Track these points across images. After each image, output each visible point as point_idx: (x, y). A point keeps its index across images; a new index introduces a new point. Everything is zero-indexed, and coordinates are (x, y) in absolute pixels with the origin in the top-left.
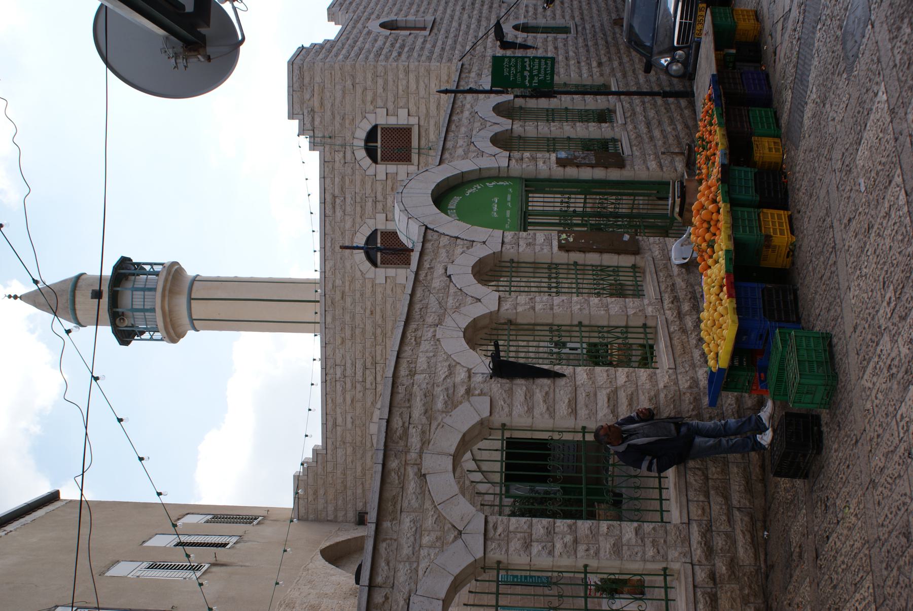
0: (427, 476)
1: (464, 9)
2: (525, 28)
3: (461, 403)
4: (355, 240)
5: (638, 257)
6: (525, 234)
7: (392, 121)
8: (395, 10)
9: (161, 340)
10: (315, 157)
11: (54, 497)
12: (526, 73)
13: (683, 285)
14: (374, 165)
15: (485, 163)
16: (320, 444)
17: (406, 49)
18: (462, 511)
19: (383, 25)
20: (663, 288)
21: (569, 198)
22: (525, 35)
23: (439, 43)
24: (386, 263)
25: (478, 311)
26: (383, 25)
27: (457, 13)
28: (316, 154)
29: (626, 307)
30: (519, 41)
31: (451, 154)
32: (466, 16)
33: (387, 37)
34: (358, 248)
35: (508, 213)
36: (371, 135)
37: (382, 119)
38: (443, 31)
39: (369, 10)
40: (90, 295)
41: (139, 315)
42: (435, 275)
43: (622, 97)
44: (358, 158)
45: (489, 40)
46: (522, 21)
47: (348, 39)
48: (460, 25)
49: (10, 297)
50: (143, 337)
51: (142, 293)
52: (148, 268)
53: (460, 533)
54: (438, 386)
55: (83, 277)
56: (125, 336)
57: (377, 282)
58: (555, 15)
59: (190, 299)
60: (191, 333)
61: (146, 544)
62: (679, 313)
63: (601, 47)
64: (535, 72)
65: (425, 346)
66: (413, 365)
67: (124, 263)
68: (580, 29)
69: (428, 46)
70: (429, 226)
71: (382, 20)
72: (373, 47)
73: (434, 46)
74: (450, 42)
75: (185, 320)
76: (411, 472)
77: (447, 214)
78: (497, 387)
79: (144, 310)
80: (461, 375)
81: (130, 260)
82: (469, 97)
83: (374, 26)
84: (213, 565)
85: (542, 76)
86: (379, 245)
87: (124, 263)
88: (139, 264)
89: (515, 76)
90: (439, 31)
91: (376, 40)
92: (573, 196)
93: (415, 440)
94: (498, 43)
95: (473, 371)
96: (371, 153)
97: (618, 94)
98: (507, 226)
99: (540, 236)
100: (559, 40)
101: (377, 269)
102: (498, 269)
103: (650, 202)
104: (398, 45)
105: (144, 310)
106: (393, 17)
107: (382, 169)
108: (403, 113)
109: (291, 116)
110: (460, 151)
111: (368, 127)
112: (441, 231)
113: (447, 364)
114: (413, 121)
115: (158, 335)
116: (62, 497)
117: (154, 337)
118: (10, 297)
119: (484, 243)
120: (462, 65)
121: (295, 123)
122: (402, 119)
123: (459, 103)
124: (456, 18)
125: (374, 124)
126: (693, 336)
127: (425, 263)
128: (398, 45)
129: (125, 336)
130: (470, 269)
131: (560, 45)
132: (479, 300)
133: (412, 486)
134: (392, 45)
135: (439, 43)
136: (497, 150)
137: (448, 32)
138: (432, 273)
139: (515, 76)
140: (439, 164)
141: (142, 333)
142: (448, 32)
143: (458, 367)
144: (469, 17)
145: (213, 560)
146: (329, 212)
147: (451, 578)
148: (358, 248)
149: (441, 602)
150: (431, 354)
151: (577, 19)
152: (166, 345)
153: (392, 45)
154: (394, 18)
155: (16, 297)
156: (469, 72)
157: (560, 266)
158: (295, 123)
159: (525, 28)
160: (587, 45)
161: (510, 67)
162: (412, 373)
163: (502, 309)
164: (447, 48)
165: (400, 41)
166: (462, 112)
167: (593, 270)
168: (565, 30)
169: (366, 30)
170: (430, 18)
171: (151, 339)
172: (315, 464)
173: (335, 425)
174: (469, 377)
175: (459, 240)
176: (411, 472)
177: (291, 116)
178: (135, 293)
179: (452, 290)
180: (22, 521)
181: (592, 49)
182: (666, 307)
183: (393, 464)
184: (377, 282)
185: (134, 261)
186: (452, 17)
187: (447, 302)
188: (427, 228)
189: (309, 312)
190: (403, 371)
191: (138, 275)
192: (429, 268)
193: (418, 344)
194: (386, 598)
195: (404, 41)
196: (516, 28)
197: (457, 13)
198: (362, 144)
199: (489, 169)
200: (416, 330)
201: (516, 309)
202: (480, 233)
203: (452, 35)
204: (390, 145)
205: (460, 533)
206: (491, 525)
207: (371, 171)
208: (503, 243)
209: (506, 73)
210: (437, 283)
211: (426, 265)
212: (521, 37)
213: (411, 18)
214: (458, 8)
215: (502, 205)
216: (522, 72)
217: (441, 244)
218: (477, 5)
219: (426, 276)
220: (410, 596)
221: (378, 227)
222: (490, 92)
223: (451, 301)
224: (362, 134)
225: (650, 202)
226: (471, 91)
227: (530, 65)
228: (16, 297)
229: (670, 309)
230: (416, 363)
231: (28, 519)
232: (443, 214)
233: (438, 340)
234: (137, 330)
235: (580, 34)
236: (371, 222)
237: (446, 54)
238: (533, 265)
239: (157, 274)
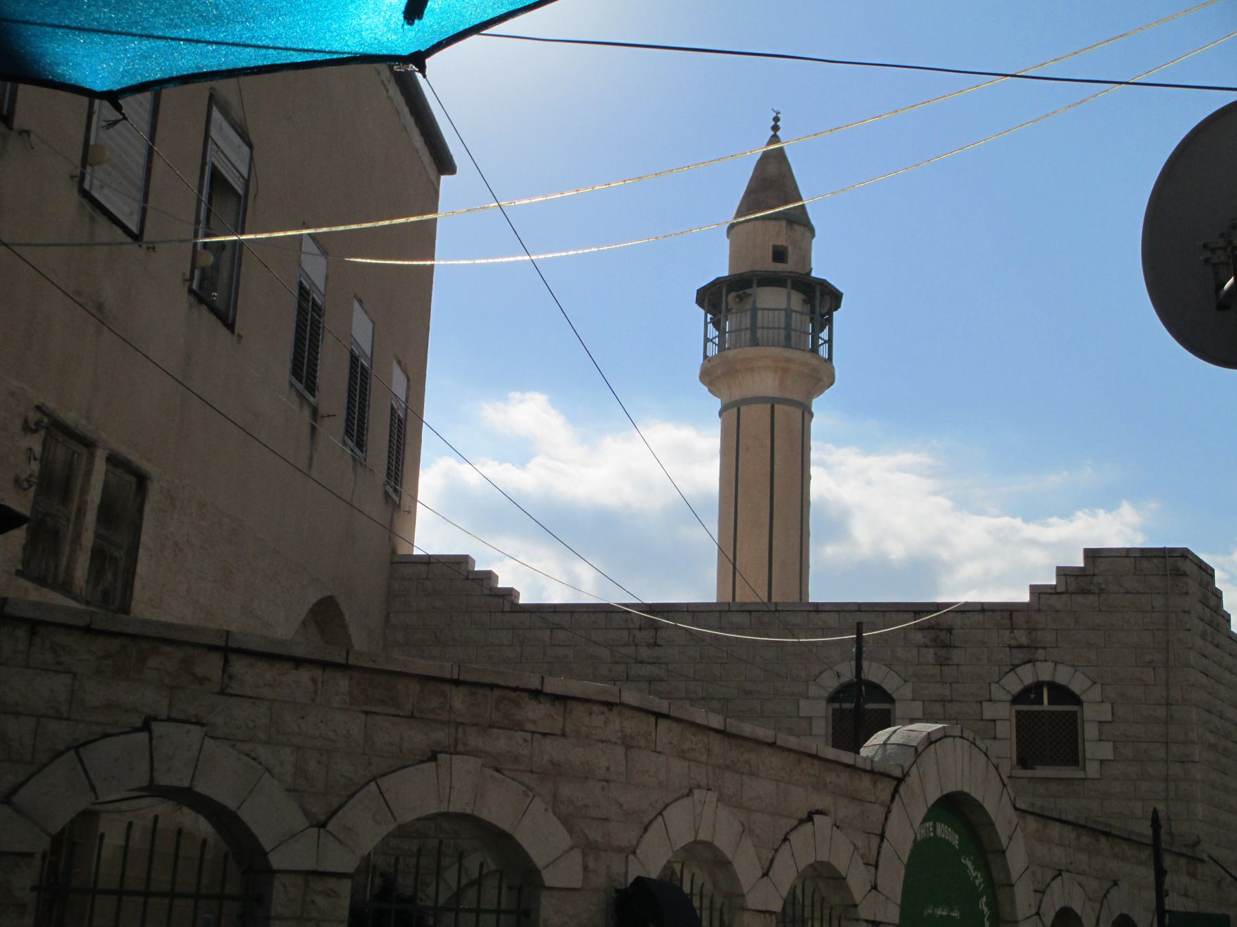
0: (433, 764)
3: (570, 832)
4: (875, 665)
7: (1090, 731)
9: (705, 356)
11: (445, 164)
14: (1009, 698)
16: (521, 602)
18: (365, 831)
24: (838, 717)
25: (746, 868)
28: (1025, 597)
34: (859, 668)
36: (1061, 693)
37: (1093, 713)
40: (780, 243)
41: (746, 320)
44: (1019, 670)
49: (776, 119)
50: (710, 326)
51: (783, 325)
52: (824, 335)
53: (322, 825)
54: (603, 789)
55: (808, 234)
57: (803, 703)
59: (772, 402)
60: (716, 404)
61: (356, 305)
67: (833, 297)
75: (736, 395)
76: (440, 736)
77: (925, 820)
79: (753, 327)
81: (837, 306)
84: (315, 413)
86: (870, 706)
87: (833, 297)
88: (830, 322)
93: (501, 742)
95: (631, 857)
96: (1029, 694)
101: (824, 703)
102: (826, 912)
105: (753, 327)
107: (1003, 713)
108: (1106, 750)
111: (1076, 688)
112: (896, 807)
114: (1092, 770)
115: (713, 350)
116: (444, 179)
117: (709, 344)
118: (776, 119)
119: (875, 887)
120: (1202, 861)
122: (1095, 749)
125: (1083, 697)
130: (825, 859)
132: (766, 874)
133: (417, 738)
141: (717, 325)
145: (323, 410)
147: (231, 804)
148: (859, 668)
149: (186, 784)
152: (696, 363)
155: (775, 128)
171: (707, 340)
172: (486, 592)
173: (555, 627)
174: (620, 850)
175: (875, 841)
176: (440, 736)
180: (406, 111)
183: (458, 700)
184: (803, 703)
188: (900, 781)
189: (753, 592)
191: (812, 321)
194: (202, 681)
199: (1012, 902)
202: (893, 880)
204: (1048, 732)
205: (322, 825)
206: (331, 883)
207: (997, 692)
220: (202, 725)
221: (898, 705)
222: (1161, 910)
224: (1063, 676)
226: (1160, 873)
228: (775, 128)
231: (410, 121)
232: (924, 811)
234: (722, 316)
236: (907, 691)
239: (815, 349)
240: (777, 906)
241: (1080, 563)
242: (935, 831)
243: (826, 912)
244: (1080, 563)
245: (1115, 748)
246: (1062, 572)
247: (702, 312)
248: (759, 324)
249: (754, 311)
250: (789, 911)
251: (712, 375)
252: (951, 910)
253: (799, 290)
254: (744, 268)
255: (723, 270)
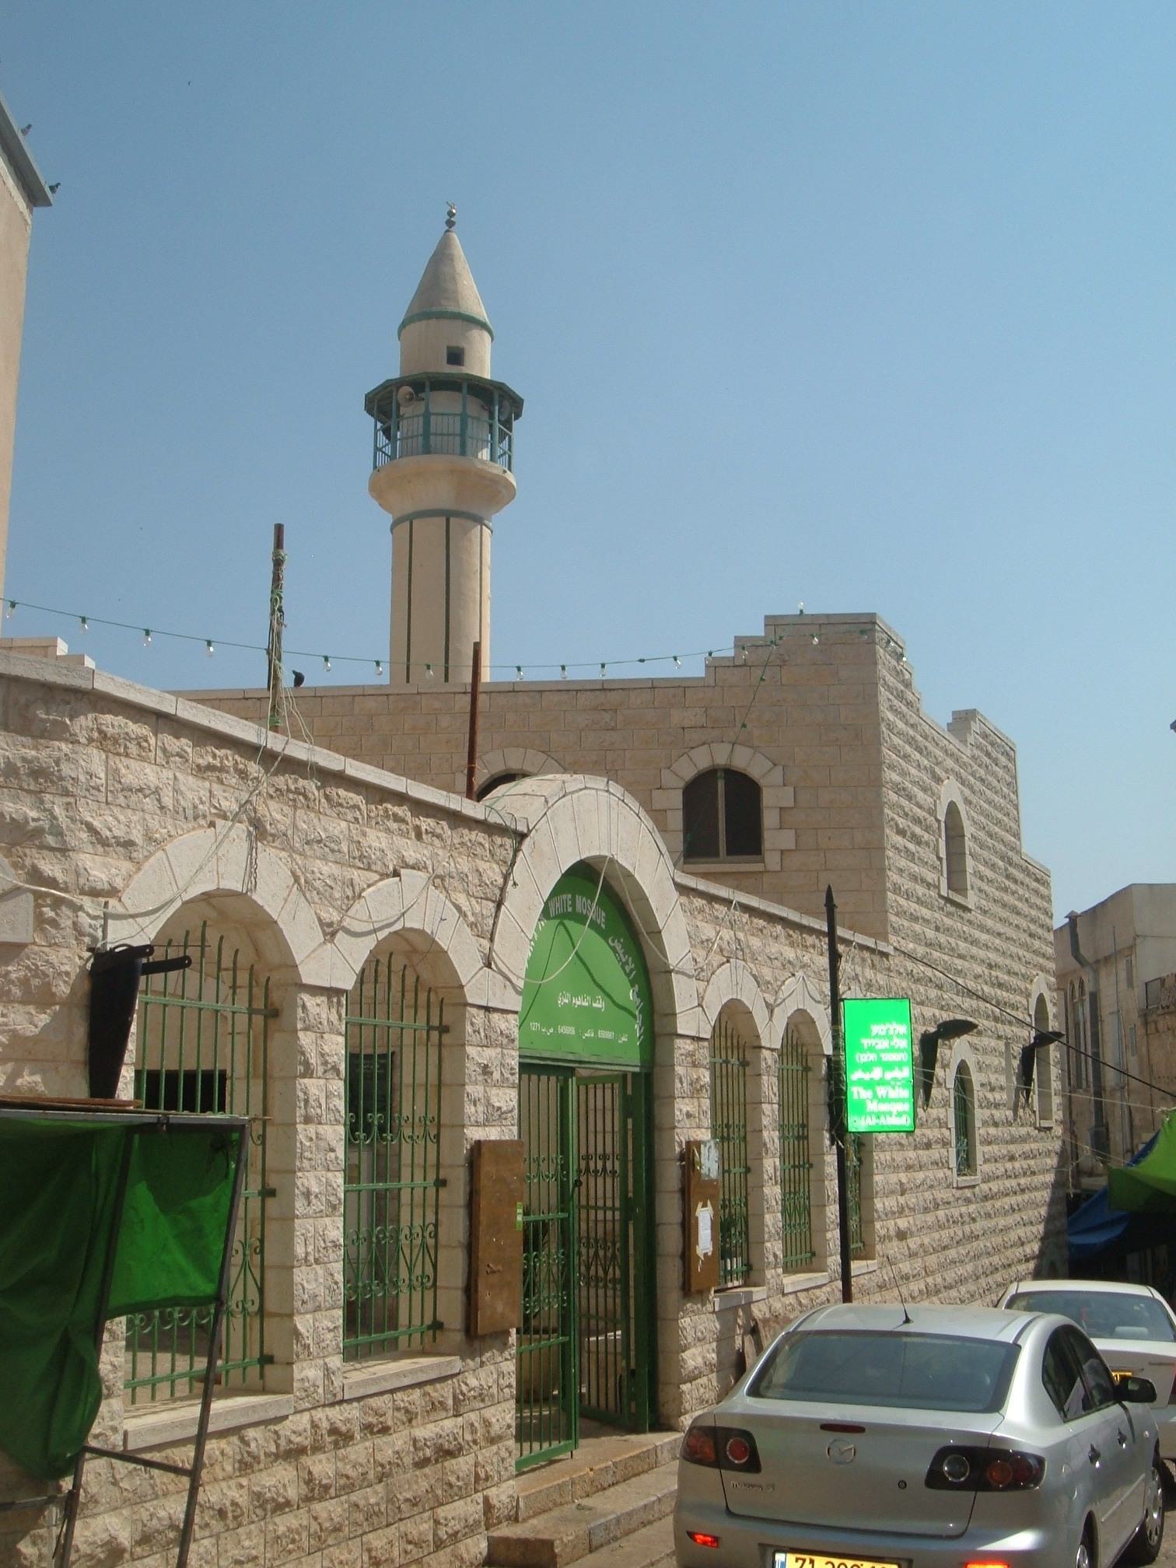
1: (990, 966)
2: (963, 1084)
5: (459, 1337)
6: (515, 1063)
8: (982, 835)
9: (375, 467)
10: (694, 669)
12: (877, 1073)
13: (387, 1454)
15: (683, 992)
17: (912, 847)
19: (952, 809)
20: (374, 1402)
21: (613, 1172)
22: (951, 1084)
23: (925, 912)
25: (300, 934)
26: (952, 809)
27: (981, 953)
29: (318, 1309)
30: (939, 1071)
31: (701, 911)
32: (979, 970)
33: (932, 812)
35: (569, 1030)
38: (948, 921)
39: (978, 786)
42: (400, 842)
43: (839, 1284)
44: (693, 753)
45: (937, 1012)
46: (976, 1078)
47: (926, 738)
48: (961, 957)
56: (382, 404)
58: (990, 1143)
62: (301, 1451)
63: (936, 1236)
64: (881, 1091)
65: (194, 789)
66: (133, 749)
68: (968, 1193)
69: (920, 890)
70: (527, 842)
71: (962, 807)
72: (913, 783)
73: (919, 901)
74: (930, 934)
75: (409, 508)
78: (69, 963)
79: (426, 434)
80: (98, 868)
81: (518, 416)
82: (824, 961)
83: (950, 791)
85: (872, 1106)
89: (871, 1049)
90: (949, 915)
91: (925, 790)
92: (617, 1180)
94: (932, 1030)
97: (846, 1276)
98: (534, 1026)
99: (507, 1098)
100: (944, 1151)
102: (423, 997)
103: (611, 1358)
104: (918, 830)
105: (426, 434)
106: (969, 829)
108: (787, 840)
109: (771, 622)
110: (708, 931)
113: (137, 836)
114: (772, 860)
121: (758, 630)
123: (811, 940)
124: (974, 950)
126: (234, 1494)
127: (431, 822)
128: (918, 830)
129: (382, 404)
131: (936, 1153)
134: (918, 821)
135: (925, 912)
136: (713, 1016)
137: (948, 930)
138: (404, 834)
139: (871, 1049)
140: (676, 884)
141: (387, 432)
142: (948, 930)
143: (126, 866)
144: (977, 977)
146: (583, 698)
150: (167, 801)
151: (985, 1187)
153: (918, 821)
154: (968, 835)
156: (873, 966)
157: (432, 1147)
158: (758, 630)
159: (963, 1084)
160: (937, 1207)
161: (888, 1037)
162: (104, 740)
163: (306, 997)
164: (917, 928)
165: (926, 836)
166: (792, 945)
167: (423, 1228)
168: (966, 1163)
169: (943, 775)
170: (972, 900)
171: (377, 449)
177: (771, 622)
178: (458, 418)
179: (359, 876)
181: (930, 1218)
182: (319, 1414)
185: (515, 424)
186: (975, 942)
187: (324, 858)
188: (522, 836)
190: (113, 723)
192: (418, 829)
193: (201, 771)
195: (927, 844)
196: (963, 1068)
197: (981, 953)
198: (721, 760)
200: (243, 774)
201: (306, 1029)
203: (943, 939)
207: (668, 778)
208: (487, 1009)
209: (876, 1029)
210: (376, 840)
211: (426, 823)
212: (945, 1075)
213: (970, 863)
214: (993, 957)
215: (589, 1017)
216: (879, 1063)
217: (482, 865)
218: (999, 992)
219: (397, 819)
223: (326, 870)
225: (611, 1358)
227: (895, 1079)
229: (314, 1426)
230: (143, 759)
233: (212, 825)
235: (958, 1193)
237: (906, 924)
238: (433, 1078)
240: (348, 983)
241: (760, 632)
242: (574, 905)
243: (423, 997)
244: (760, 632)
245: (797, 836)
246: (741, 643)
247: (372, 420)
248: (432, 430)
249: (427, 416)
250: (368, 989)
251: (378, 490)
252: (594, 1000)
253: (476, 395)
254: (415, 371)
255: (393, 371)
